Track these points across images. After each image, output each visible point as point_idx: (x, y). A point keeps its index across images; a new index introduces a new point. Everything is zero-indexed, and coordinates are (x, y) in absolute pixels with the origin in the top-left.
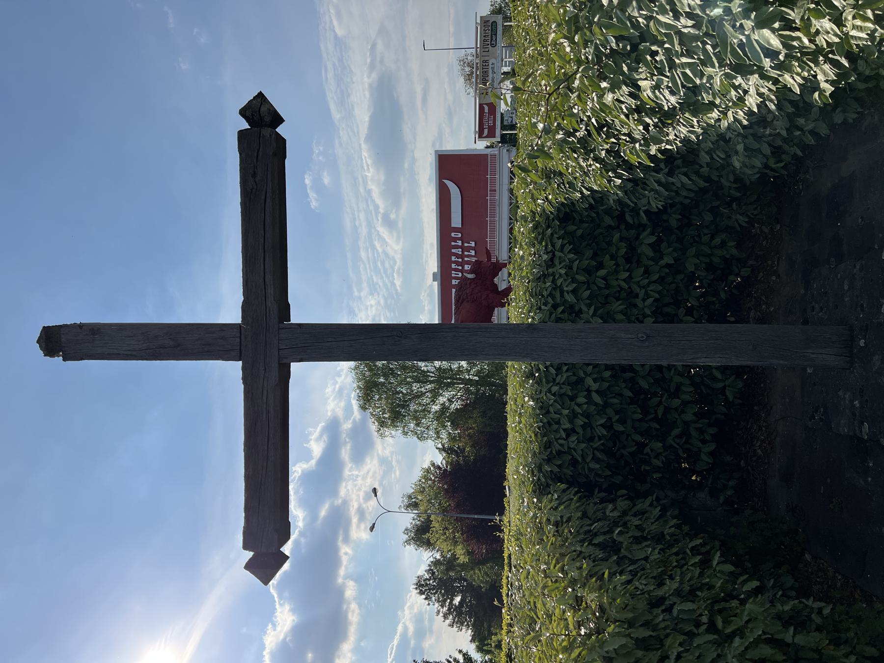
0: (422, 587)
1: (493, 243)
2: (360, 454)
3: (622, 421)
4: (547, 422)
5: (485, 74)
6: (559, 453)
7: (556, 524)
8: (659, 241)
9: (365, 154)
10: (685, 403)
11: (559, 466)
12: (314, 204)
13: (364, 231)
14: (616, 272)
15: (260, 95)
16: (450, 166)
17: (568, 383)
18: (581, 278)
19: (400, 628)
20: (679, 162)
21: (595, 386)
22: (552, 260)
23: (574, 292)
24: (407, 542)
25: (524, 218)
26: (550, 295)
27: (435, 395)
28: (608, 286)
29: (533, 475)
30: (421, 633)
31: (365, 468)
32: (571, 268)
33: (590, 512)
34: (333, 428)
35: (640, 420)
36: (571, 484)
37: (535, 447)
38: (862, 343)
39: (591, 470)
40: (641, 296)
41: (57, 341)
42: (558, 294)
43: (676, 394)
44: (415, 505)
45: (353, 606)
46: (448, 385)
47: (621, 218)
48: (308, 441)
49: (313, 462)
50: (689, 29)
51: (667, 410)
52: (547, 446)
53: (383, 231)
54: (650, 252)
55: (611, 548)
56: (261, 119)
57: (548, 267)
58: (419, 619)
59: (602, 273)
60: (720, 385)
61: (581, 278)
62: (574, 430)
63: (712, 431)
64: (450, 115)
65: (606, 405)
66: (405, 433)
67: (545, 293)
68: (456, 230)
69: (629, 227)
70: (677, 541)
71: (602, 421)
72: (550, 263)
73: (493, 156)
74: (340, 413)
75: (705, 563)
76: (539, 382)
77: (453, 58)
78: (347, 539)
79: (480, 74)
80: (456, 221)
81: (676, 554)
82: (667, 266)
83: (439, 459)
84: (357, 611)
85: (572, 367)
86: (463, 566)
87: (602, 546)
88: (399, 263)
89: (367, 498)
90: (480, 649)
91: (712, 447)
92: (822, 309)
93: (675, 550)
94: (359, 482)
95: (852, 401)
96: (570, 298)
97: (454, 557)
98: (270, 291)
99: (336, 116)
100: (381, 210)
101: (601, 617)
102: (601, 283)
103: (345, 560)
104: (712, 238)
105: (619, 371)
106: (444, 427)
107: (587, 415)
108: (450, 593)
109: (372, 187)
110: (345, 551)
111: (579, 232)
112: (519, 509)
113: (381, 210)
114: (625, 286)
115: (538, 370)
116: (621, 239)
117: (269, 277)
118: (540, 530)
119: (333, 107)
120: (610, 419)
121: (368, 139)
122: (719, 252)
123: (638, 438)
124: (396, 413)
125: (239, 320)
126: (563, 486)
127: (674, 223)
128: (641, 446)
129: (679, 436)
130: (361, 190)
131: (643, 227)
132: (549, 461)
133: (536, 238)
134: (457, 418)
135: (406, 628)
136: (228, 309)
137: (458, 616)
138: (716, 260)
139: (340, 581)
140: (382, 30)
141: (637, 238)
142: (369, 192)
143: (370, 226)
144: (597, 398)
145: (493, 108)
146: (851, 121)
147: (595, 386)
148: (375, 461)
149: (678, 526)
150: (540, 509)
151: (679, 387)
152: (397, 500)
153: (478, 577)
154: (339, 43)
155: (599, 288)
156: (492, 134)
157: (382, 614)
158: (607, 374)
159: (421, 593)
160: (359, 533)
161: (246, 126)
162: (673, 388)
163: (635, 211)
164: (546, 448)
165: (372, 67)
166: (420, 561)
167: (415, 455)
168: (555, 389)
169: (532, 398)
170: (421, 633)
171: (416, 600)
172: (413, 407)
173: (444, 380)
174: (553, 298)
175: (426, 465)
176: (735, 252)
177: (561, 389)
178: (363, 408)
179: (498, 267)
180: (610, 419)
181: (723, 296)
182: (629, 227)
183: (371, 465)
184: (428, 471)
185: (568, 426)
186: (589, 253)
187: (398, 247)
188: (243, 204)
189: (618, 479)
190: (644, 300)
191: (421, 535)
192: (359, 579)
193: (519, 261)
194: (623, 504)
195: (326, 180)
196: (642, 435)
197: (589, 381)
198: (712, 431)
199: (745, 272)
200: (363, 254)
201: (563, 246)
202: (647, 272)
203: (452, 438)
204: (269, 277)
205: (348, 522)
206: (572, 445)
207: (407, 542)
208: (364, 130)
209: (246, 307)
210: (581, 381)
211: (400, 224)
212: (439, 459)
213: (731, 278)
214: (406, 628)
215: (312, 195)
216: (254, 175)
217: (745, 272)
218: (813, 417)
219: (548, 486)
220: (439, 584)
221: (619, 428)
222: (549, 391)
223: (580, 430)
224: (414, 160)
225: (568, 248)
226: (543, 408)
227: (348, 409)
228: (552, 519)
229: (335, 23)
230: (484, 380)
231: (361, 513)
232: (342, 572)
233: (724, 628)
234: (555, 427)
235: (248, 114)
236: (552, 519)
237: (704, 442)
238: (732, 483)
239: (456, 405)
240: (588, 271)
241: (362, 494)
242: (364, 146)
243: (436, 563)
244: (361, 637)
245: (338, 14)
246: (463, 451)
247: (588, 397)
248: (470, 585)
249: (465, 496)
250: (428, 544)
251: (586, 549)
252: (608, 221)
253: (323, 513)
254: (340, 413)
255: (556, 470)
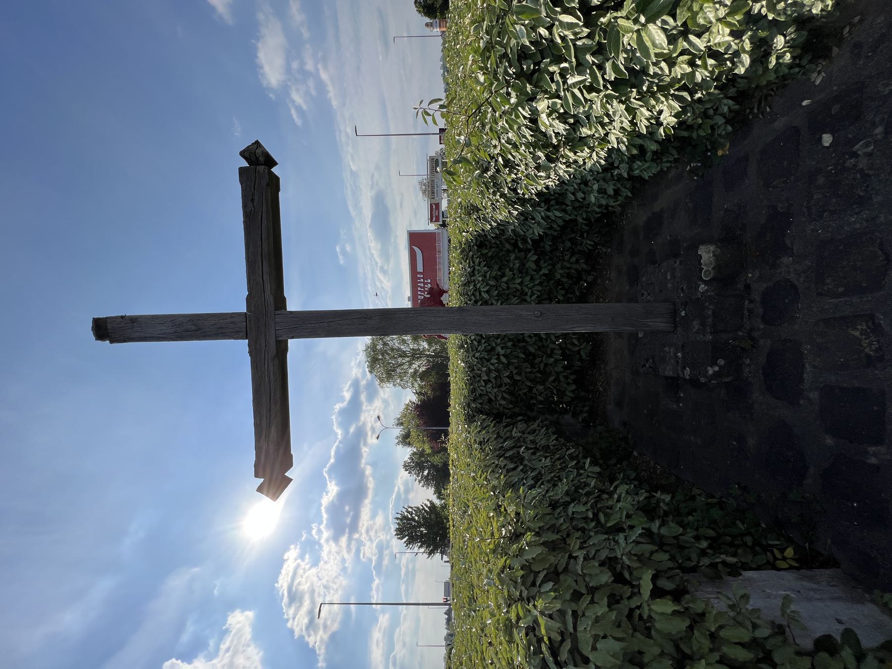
0: (407, 467)
1: (440, 280)
2: (371, 398)
3: (519, 374)
4: (473, 377)
5: (433, 187)
6: (481, 395)
7: (480, 443)
8: (539, 260)
9: (369, 234)
10: (556, 361)
11: (481, 404)
12: (342, 262)
13: (369, 275)
14: (513, 279)
15: (257, 142)
16: (416, 239)
17: (485, 350)
18: (492, 283)
19: (396, 489)
20: (553, 202)
21: (502, 352)
22: (473, 272)
23: (487, 292)
24: (398, 444)
25: (455, 248)
26: (473, 294)
27: (411, 364)
28: (508, 288)
29: (465, 410)
30: (407, 491)
31: (375, 405)
32: (485, 276)
33: (502, 434)
34: (356, 384)
35: (530, 372)
36: (487, 414)
37: (466, 392)
38: (683, 314)
39: (500, 405)
40: (529, 294)
41: (104, 329)
42: (477, 294)
43: (550, 356)
44: (402, 424)
45: (370, 479)
46: (418, 358)
47: (515, 245)
48: (342, 392)
49: (345, 403)
50: (584, 40)
51: (546, 365)
52: (473, 391)
53: (380, 275)
54: (533, 266)
55: (518, 459)
56: (257, 159)
57: (471, 276)
58: (406, 484)
59: (505, 279)
60: (577, 349)
61: (492, 283)
62: (489, 381)
63: (573, 377)
64: (415, 213)
65: (509, 363)
66: (395, 385)
67: (469, 293)
68: (420, 273)
69: (520, 250)
70: (558, 450)
71: (507, 374)
72: (472, 274)
73: (439, 234)
74: (359, 376)
75: (579, 467)
76: (467, 351)
77: (415, 181)
78: (365, 444)
79: (431, 190)
80: (420, 268)
81: (559, 459)
82: (544, 275)
83: (414, 398)
84: (372, 482)
85: (488, 338)
86: (428, 455)
87: (511, 459)
88: (390, 293)
89: (375, 422)
90: (439, 498)
91: (574, 387)
92: (649, 294)
93: (557, 456)
94: (371, 412)
95: (675, 354)
96: (485, 296)
97: (423, 450)
98: (268, 287)
99: (353, 213)
100: (379, 264)
101: (518, 521)
102: (504, 286)
103: (365, 455)
104: (571, 257)
105: (518, 340)
106: (416, 381)
107: (497, 370)
108: (422, 469)
109: (374, 252)
110: (365, 450)
111: (490, 254)
112: (458, 431)
113: (379, 264)
114: (519, 288)
115: (467, 343)
116: (516, 258)
117: (266, 277)
118: (469, 447)
119: (351, 208)
120: (511, 372)
121: (370, 226)
122: (574, 266)
123: (529, 384)
124: (389, 374)
125: (244, 309)
126: (484, 417)
127: (548, 248)
128: (531, 389)
129: (554, 381)
130: (368, 252)
131: (529, 250)
132: (474, 400)
133: (463, 258)
134: (423, 376)
135: (399, 489)
136: (233, 297)
137: (427, 481)
138: (573, 271)
139: (363, 466)
140: (377, 168)
141: (525, 258)
142: (372, 255)
143: (373, 272)
144: (503, 360)
145: (438, 206)
146: (665, 169)
147: (502, 352)
148: (380, 401)
149: (556, 439)
150: (469, 433)
151: (553, 350)
152: (392, 421)
153: (437, 460)
154: (354, 175)
155: (504, 290)
156: (437, 220)
157: (385, 482)
158: (510, 344)
159: (406, 470)
160: (372, 440)
161: (246, 164)
162: (549, 352)
163: (524, 241)
164: (472, 393)
165: (372, 187)
166: (405, 453)
167: (403, 396)
168: (477, 355)
169: (463, 361)
170: (407, 491)
171: (404, 474)
172: (398, 371)
173: (416, 355)
174: (475, 297)
175: (407, 402)
176: (585, 266)
177: (482, 350)
178: (371, 372)
179: (442, 292)
180: (511, 372)
181: (577, 293)
182: (520, 250)
183: (378, 403)
184: (408, 405)
185: (486, 378)
186: (496, 267)
187: (389, 284)
188: (245, 222)
189: (517, 410)
190: (531, 297)
191: (405, 439)
192: (374, 465)
193: (452, 274)
194: (521, 426)
195: (348, 248)
196: (530, 381)
197: (499, 349)
198: (573, 377)
199: (590, 278)
200: (370, 288)
201: (480, 263)
202: (532, 279)
203: (421, 387)
204: (266, 277)
205: (366, 435)
206: (489, 390)
207: (398, 444)
208: (368, 222)
209: (249, 300)
210: (493, 349)
211: (390, 272)
212: (414, 398)
213: (582, 282)
214: (399, 489)
215: (341, 257)
216: (252, 200)
217: (590, 278)
218: (645, 366)
219: (474, 416)
220: (417, 464)
221: (517, 378)
222: (474, 356)
223: (494, 381)
224: (396, 237)
225: (483, 263)
226: (471, 367)
227: (364, 374)
228: (478, 440)
229: (351, 163)
230: (437, 355)
231: (373, 430)
232: (363, 461)
233: (606, 521)
234: (478, 379)
235: (247, 155)
236: (478, 440)
237: (568, 384)
238: (586, 409)
239: (423, 369)
240: (495, 278)
241: (373, 419)
242: (369, 230)
243: (414, 454)
244: (376, 494)
245: (352, 157)
246: (426, 393)
247: (498, 359)
248: (432, 464)
249: (431, 415)
250: (409, 444)
251: (502, 462)
252: (508, 246)
253: (352, 430)
254: (359, 376)
255: (479, 406)
